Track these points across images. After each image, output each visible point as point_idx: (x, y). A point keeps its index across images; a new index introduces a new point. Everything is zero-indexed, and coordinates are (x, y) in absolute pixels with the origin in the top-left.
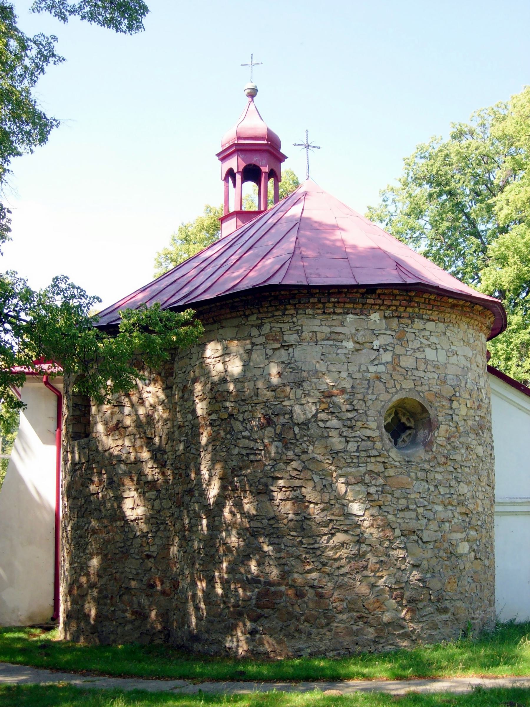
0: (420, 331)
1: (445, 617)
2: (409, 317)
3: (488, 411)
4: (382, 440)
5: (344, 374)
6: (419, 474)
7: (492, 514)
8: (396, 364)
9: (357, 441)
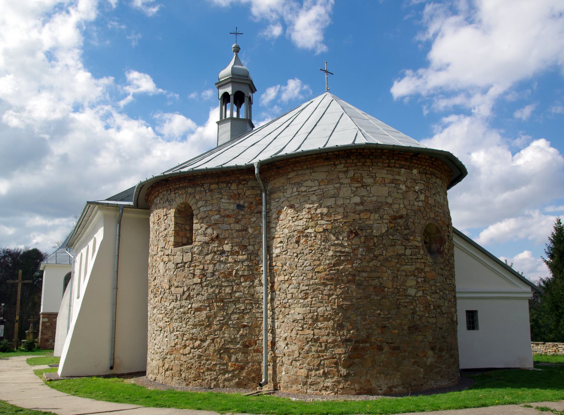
4: (423, 249)
5: (402, 206)
8: (426, 202)
9: (411, 249)
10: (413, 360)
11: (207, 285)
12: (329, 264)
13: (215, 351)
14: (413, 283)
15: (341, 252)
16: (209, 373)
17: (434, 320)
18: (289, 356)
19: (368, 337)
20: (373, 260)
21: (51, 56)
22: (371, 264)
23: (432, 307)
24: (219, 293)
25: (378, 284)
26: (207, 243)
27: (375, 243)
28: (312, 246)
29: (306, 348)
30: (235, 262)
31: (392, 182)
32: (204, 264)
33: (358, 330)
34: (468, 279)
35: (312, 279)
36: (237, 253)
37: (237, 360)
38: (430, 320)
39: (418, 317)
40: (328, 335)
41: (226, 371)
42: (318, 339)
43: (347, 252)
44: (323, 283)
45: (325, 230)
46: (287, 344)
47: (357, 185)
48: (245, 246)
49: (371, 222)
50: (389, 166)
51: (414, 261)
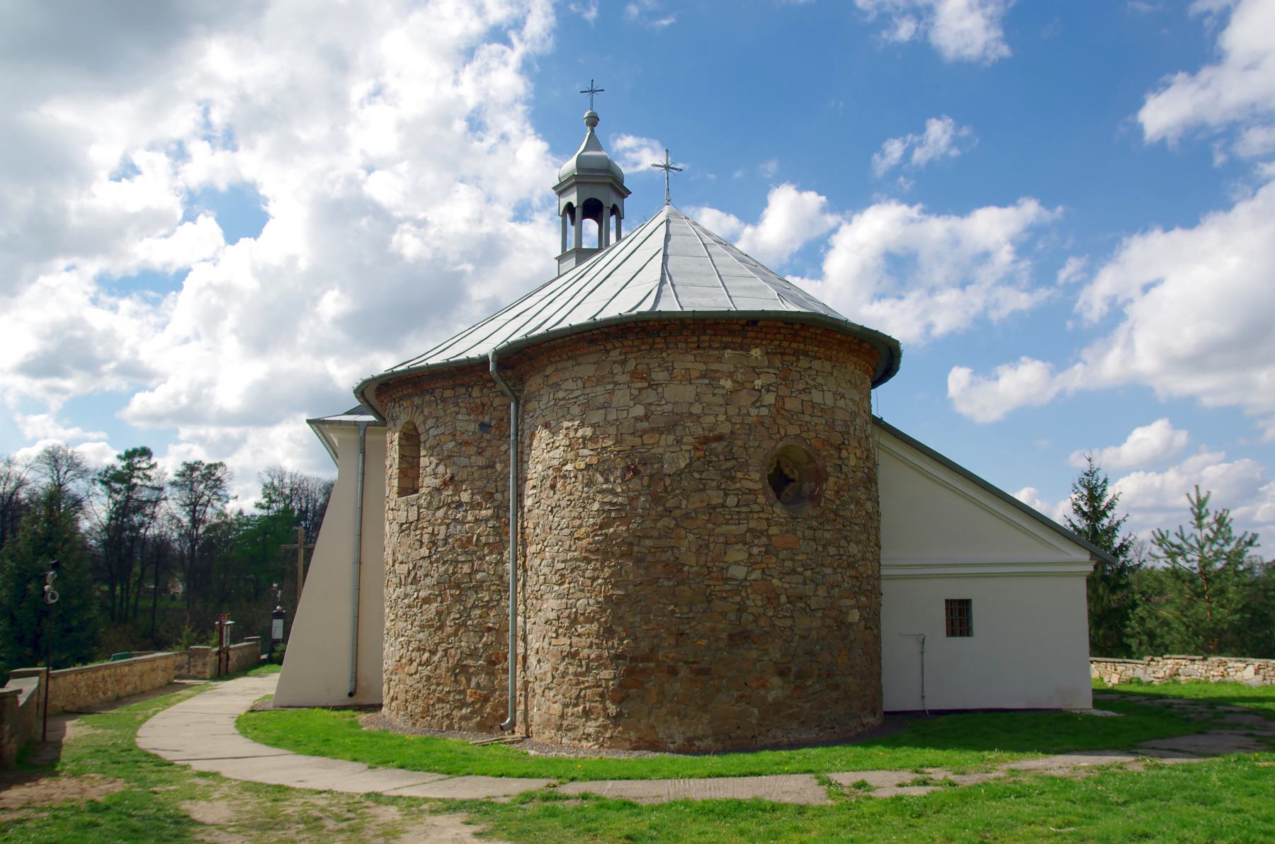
0: (805, 370)
1: (834, 694)
2: (794, 355)
3: (876, 465)
4: (765, 494)
5: (722, 418)
6: (807, 532)
7: (879, 578)
8: (779, 408)
10: (736, 694)
11: (437, 561)
12: (594, 524)
13: (448, 670)
14: (742, 556)
15: (610, 503)
16: (440, 705)
17: (788, 623)
18: (541, 680)
19: (652, 650)
20: (662, 517)
21: (476, 124)
22: (659, 525)
23: (783, 599)
24: (454, 573)
25: (672, 559)
26: (438, 490)
27: (666, 487)
28: (571, 494)
29: (561, 668)
30: (477, 520)
31: (703, 376)
32: (434, 525)
33: (635, 639)
34: (918, 545)
35: (569, 550)
36: (479, 506)
37: (478, 684)
38: (778, 623)
39: (751, 618)
40: (590, 647)
41: (463, 704)
42: (577, 653)
43: (621, 504)
44: (585, 558)
45: (588, 466)
46: (539, 661)
47: (639, 385)
48: (491, 494)
49: (661, 450)
50: (698, 347)
51: (743, 516)
